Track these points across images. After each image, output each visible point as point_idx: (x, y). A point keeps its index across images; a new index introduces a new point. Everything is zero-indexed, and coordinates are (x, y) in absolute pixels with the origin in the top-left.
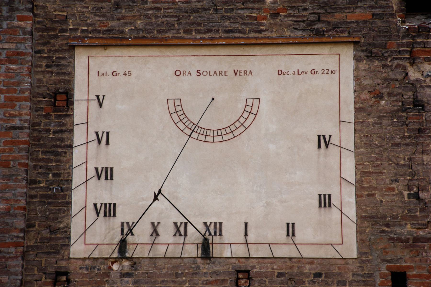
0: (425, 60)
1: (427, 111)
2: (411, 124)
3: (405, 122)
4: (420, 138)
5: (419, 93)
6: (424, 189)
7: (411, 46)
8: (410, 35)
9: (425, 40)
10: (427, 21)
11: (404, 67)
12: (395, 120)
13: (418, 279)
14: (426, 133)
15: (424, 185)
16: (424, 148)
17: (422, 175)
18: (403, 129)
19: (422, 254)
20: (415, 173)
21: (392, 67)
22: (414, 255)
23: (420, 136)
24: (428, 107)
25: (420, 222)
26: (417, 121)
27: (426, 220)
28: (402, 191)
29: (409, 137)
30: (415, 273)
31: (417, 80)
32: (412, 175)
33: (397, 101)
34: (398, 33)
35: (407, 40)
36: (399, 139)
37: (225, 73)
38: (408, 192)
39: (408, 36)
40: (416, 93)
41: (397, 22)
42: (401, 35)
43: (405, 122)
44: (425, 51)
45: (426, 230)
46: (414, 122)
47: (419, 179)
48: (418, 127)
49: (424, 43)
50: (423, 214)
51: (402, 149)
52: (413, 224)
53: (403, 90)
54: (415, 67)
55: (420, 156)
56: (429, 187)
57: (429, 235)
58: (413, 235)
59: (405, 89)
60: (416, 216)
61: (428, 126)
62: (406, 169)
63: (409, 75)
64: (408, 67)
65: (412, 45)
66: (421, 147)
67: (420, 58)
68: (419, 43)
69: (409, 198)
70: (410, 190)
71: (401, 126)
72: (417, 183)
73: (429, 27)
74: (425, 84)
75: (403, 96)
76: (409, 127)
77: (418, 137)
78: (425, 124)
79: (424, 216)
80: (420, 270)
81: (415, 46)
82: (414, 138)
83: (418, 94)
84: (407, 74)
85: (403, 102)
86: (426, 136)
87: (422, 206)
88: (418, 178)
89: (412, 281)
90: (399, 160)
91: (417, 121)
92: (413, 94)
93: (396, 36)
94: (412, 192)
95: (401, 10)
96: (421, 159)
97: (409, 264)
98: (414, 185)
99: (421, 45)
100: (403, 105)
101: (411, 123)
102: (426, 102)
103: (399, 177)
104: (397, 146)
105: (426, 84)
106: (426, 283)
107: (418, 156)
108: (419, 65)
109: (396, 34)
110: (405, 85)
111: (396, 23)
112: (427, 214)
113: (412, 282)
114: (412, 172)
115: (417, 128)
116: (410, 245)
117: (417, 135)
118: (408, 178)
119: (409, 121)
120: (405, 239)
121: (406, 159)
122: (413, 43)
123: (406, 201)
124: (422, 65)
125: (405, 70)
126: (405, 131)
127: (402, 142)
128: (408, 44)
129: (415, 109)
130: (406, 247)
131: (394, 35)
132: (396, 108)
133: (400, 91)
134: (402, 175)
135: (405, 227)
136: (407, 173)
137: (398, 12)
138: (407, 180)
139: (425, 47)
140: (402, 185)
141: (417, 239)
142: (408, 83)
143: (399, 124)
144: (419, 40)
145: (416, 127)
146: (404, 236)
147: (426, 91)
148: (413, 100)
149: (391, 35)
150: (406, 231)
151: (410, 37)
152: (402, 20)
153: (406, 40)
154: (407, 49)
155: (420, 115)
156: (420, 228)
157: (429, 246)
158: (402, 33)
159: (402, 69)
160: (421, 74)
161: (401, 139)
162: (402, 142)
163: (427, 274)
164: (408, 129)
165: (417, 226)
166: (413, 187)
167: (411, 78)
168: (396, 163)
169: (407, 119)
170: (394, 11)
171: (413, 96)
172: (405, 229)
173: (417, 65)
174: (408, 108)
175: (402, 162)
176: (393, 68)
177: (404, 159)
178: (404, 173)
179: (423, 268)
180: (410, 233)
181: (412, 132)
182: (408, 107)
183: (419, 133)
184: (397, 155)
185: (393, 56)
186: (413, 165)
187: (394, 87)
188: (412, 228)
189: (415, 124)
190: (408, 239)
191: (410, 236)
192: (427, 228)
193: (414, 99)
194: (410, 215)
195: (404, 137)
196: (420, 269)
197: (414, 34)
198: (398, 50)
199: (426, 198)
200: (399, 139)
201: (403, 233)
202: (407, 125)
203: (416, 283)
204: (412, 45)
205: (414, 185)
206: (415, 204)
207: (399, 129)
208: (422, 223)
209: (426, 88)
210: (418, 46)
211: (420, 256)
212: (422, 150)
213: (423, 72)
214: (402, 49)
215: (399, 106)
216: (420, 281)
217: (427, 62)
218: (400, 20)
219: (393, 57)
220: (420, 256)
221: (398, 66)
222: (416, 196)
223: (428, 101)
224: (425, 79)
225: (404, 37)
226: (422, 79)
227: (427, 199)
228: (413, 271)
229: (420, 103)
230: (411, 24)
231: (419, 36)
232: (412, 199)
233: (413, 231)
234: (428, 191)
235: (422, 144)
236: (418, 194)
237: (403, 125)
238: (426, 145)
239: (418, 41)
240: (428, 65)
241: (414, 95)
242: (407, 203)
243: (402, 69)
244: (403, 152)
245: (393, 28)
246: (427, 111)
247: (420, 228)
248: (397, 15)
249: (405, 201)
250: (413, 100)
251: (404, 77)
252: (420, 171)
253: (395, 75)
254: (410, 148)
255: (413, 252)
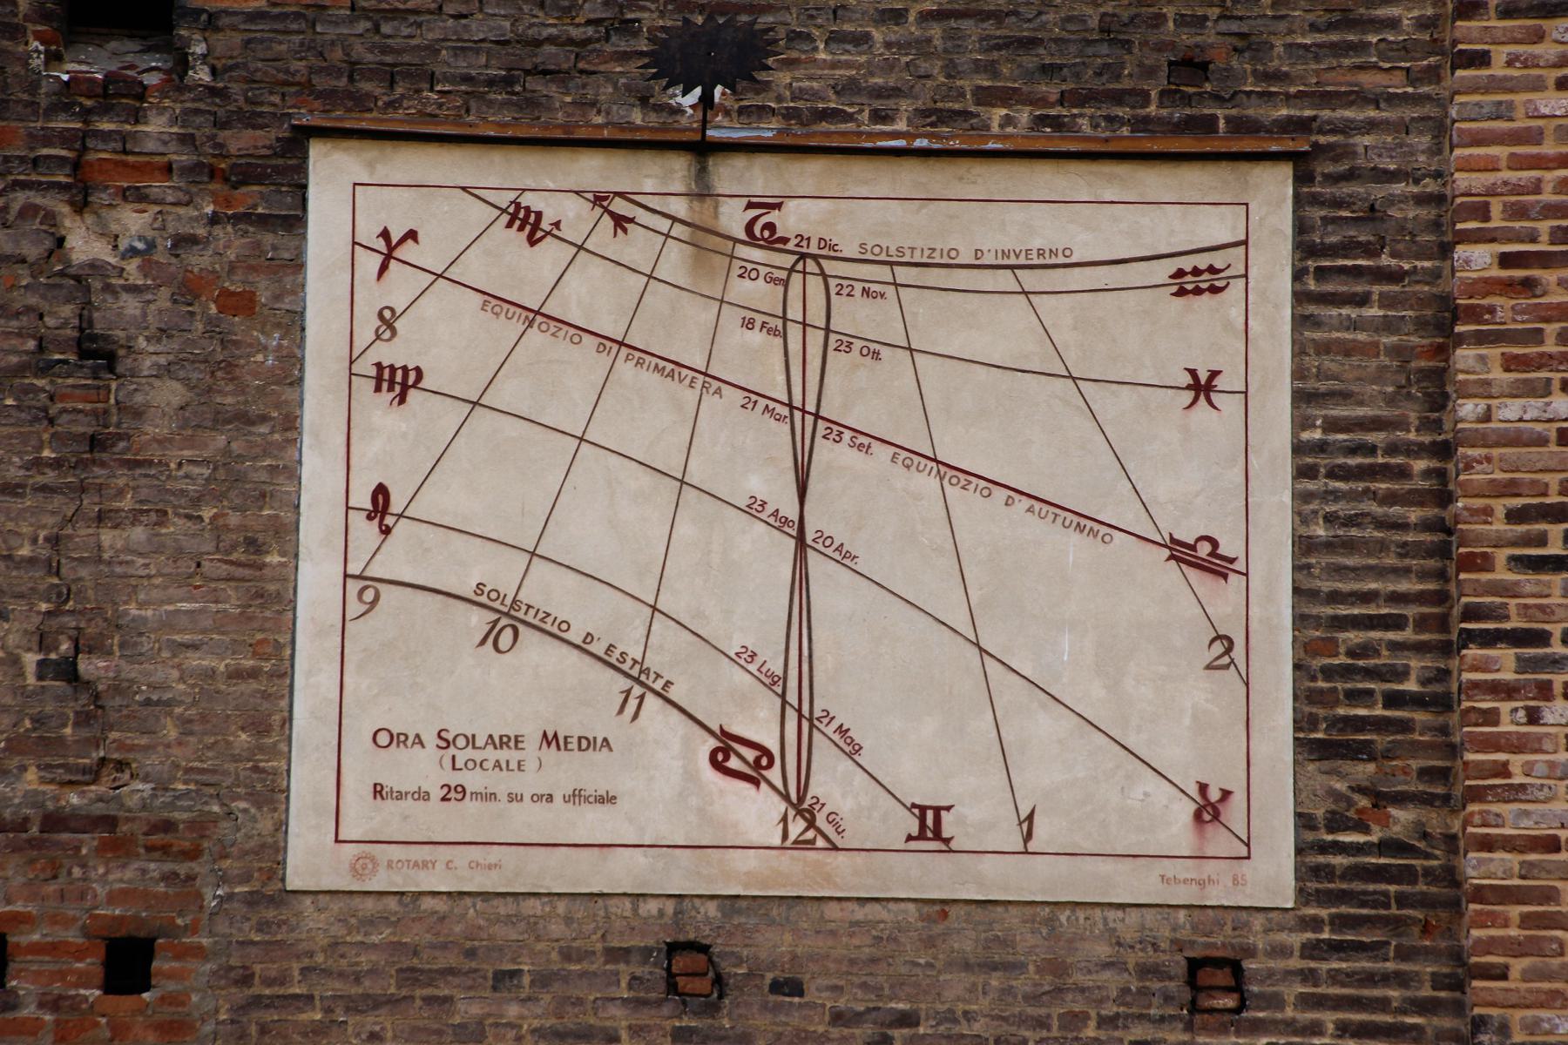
0: (124, 194)
1: (125, 376)
2: (65, 418)
3: (45, 410)
4: (95, 469)
5: (98, 309)
6: (97, 647)
7: (78, 145)
8: (74, 104)
9: (128, 127)
10: (145, 61)
11: (50, 218)
12: (9, 402)
13: (47, 958)
14: (116, 450)
15: (97, 631)
16: (107, 505)
17: (93, 597)
18: (38, 433)
19: (70, 873)
20: (69, 590)
21: (8, 213)
22: (42, 876)
23: (94, 462)
24: (129, 361)
25: (71, 760)
26: (89, 407)
27: (94, 755)
28: (19, 651)
29: (57, 464)
30: (36, 937)
31: (95, 266)
32: (59, 595)
33: (19, 335)
34: (34, 96)
35: (62, 121)
36: (20, 467)
37: (517, 742)
38: (40, 657)
39: (66, 108)
40: (90, 311)
41: (31, 57)
42: (44, 102)
43: (45, 410)
44: (125, 164)
45: (93, 788)
46: (75, 410)
47: (80, 612)
48: (90, 430)
49: (124, 137)
50: (85, 733)
51: (29, 503)
52: (48, 767)
53: (44, 297)
54: (89, 219)
55: (91, 531)
56: (112, 638)
57: (100, 805)
58: (43, 805)
59: (49, 295)
60: (61, 740)
61: (125, 426)
62: (37, 575)
63: (68, 245)
64: (65, 216)
65: (79, 142)
66: (96, 499)
67: (107, 187)
68: (106, 136)
69: (40, 678)
70: (49, 651)
71: (31, 423)
72: (73, 624)
73: (141, 83)
74: (122, 282)
75: (41, 317)
76: (60, 429)
77: (86, 466)
78: (114, 419)
79: (87, 740)
80: (57, 928)
81: (90, 143)
82: (74, 468)
83: (96, 315)
84: (61, 241)
85: (41, 340)
86: (115, 460)
87: (84, 706)
88: (79, 607)
89: (22, 966)
90: (14, 542)
91: (89, 407)
92: (78, 312)
93: (26, 107)
94: (53, 656)
95: (43, 16)
96: (92, 540)
97: (18, 907)
98: (62, 633)
99: (112, 145)
100: (41, 348)
101: (65, 415)
102: (122, 342)
103: (10, 604)
104: (10, 494)
105: (127, 280)
106: (72, 972)
107: (83, 532)
108: (104, 212)
109: (25, 97)
110: (51, 281)
111: (24, 60)
112: (98, 735)
113: (21, 970)
114: (57, 586)
115: (84, 434)
116: (29, 841)
117: (85, 456)
118: (44, 607)
119: (60, 405)
120: (13, 821)
121: (41, 541)
122: (85, 135)
123: (31, 688)
124: (114, 213)
125: (54, 225)
126: (42, 442)
127: (31, 481)
128: (65, 138)
129: (82, 367)
130: (16, 849)
131: (18, 102)
132: (14, 359)
133: (33, 300)
134: (21, 596)
135: (18, 778)
136: (42, 587)
137: (35, 23)
138: (39, 613)
139: (125, 152)
140: (18, 631)
141: (55, 821)
142: (62, 274)
143: (23, 415)
144: (106, 126)
145: (81, 429)
146: (13, 809)
147: (122, 304)
148: (76, 334)
149: (7, 101)
150: (19, 794)
151: (74, 114)
152: (47, 51)
153: (61, 123)
154: (64, 153)
155: (99, 388)
156: (71, 783)
157: (95, 843)
158: (47, 94)
159: (41, 223)
160: (109, 243)
161: (28, 469)
162: (31, 481)
163: (80, 941)
164: (53, 435)
165: (60, 775)
166: (56, 640)
167: (74, 257)
168: (5, 553)
169: (52, 398)
170: (21, 16)
171: (76, 322)
172: (19, 786)
173: (96, 213)
174: (59, 361)
175: (25, 551)
176: (11, 218)
177: (34, 541)
178: (31, 589)
179: (68, 922)
180: (32, 798)
181: (66, 445)
182: (57, 357)
183: (91, 451)
184: (10, 525)
185: (11, 173)
186: (63, 561)
187: (13, 286)
188: (42, 781)
189: (80, 416)
190: (26, 819)
191: (32, 808)
192: (94, 782)
193: (81, 330)
194: (40, 738)
195: (38, 464)
196: (56, 923)
197: (89, 103)
198: (32, 155)
199: (99, 679)
200: (20, 467)
201: (11, 799)
202: (51, 422)
203: (39, 973)
204: (79, 142)
205: (61, 630)
206: (60, 699)
207: (20, 433)
208: (78, 764)
209: (124, 296)
210: (100, 146)
211: (62, 879)
212: (100, 510)
213: (117, 237)
214: (45, 151)
215: (27, 352)
216: (51, 967)
217: (132, 206)
218: (41, 48)
219: (10, 178)
220: (61, 880)
221: (28, 211)
222: (68, 671)
223: (129, 338)
224: (123, 264)
225: (52, 110)
226: (113, 261)
227: (104, 681)
228: (32, 932)
229: (101, 344)
230: (84, 68)
231: (105, 110)
232: (52, 679)
233: (44, 793)
234: (110, 653)
235: (100, 488)
236: (75, 664)
237: (36, 419)
238: (112, 492)
239: (101, 128)
240: (135, 215)
241: (81, 316)
242: (34, 693)
243: (41, 223)
244: (33, 514)
245: (16, 75)
246: (125, 376)
247: (71, 783)
248: (29, 32)
249: (25, 687)
250: (76, 334)
251: (50, 253)
252: (88, 584)
253: (17, 242)
254: (58, 500)
255: (39, 866)
